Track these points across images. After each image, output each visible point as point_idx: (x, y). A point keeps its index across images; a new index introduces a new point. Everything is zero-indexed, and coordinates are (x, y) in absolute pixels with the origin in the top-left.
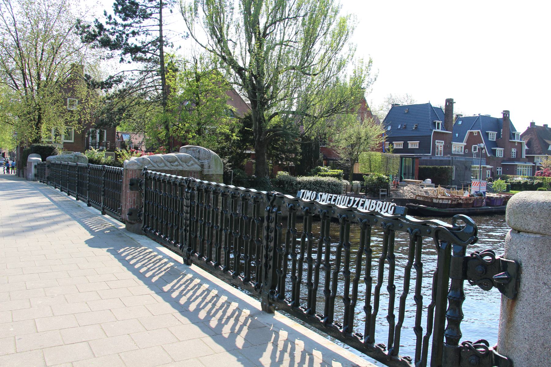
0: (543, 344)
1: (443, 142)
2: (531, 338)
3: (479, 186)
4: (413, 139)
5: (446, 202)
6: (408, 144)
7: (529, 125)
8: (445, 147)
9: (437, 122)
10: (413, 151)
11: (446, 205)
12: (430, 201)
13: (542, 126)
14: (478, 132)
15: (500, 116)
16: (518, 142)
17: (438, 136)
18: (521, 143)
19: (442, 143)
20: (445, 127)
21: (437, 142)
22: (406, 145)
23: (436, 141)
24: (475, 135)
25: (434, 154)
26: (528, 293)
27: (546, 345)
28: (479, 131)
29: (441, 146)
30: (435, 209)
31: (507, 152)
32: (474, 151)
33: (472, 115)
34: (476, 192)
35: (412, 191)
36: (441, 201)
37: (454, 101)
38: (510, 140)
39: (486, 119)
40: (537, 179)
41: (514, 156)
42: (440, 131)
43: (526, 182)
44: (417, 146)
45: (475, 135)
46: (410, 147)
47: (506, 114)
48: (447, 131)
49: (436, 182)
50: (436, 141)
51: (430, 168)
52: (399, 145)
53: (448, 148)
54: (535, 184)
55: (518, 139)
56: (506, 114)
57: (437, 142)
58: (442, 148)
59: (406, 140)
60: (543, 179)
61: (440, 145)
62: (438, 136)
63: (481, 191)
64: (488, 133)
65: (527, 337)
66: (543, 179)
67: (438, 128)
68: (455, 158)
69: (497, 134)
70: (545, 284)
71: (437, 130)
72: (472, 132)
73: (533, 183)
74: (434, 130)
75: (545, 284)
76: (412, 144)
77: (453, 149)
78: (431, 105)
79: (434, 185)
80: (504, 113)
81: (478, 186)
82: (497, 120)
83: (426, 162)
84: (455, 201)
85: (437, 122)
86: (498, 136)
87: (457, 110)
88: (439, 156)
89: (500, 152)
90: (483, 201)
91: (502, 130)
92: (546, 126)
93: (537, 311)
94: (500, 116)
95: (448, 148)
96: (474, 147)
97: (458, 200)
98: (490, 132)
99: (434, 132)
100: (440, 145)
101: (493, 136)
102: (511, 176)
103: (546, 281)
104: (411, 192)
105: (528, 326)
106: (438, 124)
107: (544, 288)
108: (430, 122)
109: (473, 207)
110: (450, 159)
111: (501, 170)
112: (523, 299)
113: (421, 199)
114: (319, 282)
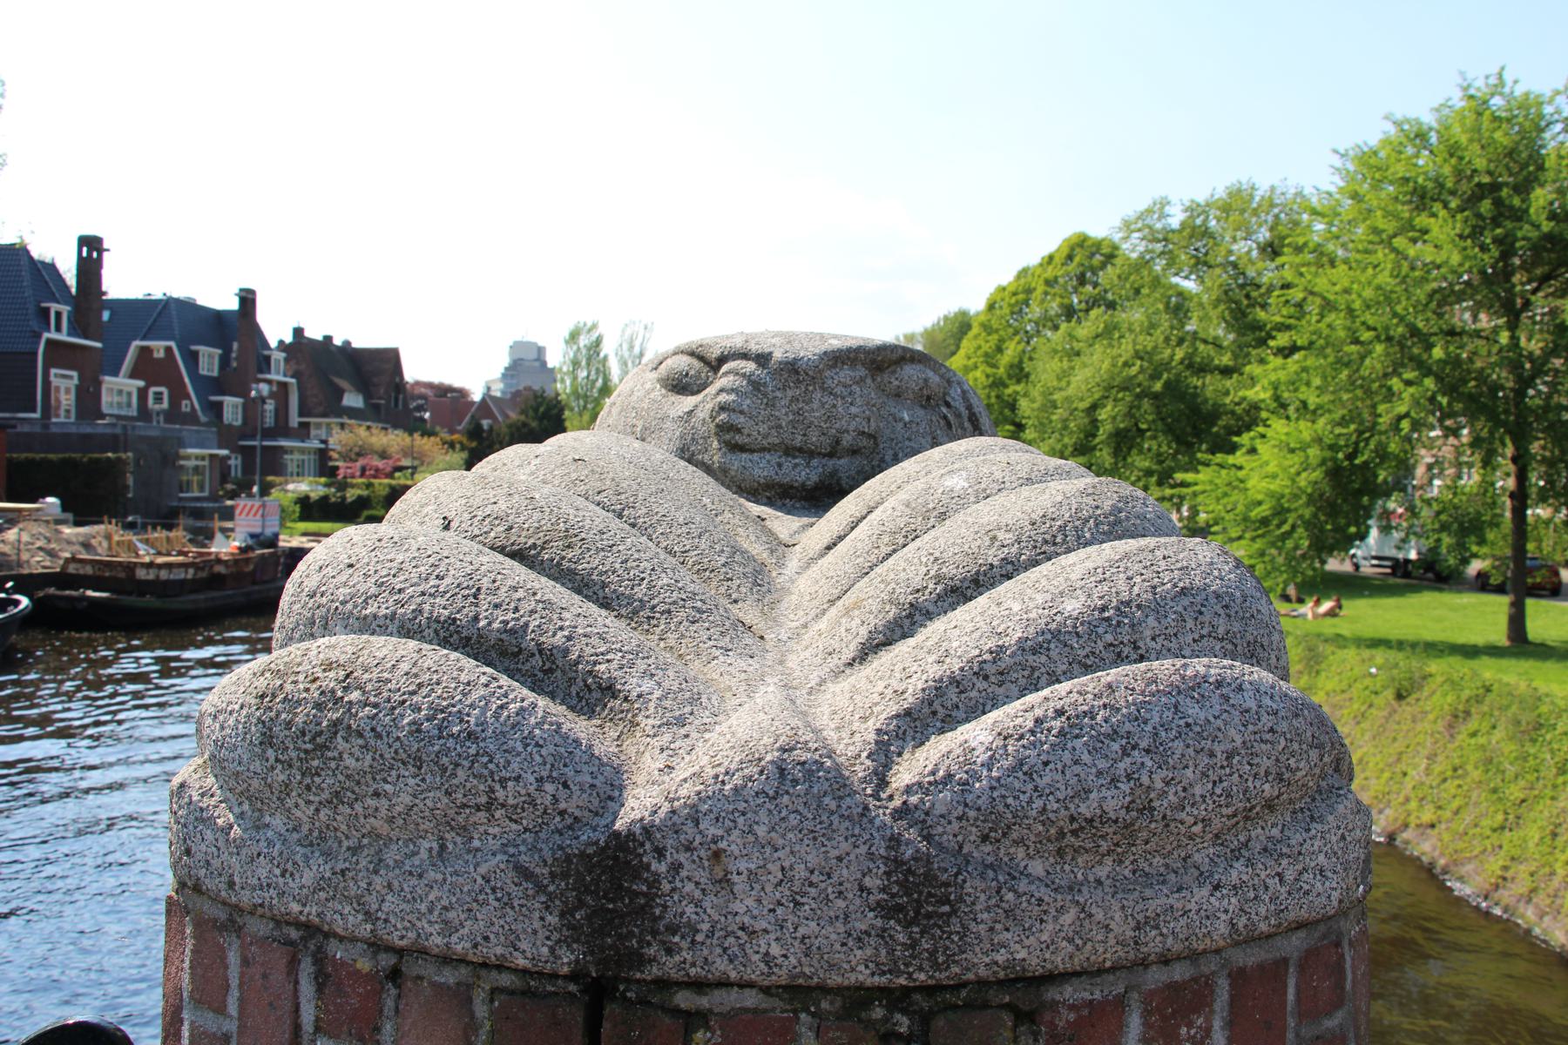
1: (75, 374)
3: (263, 516)
5: (179, 575)
8: (81, 391)
9: (54, 307)
11: (180, 587)
12: (122, 575)
13: (320, 338)
14: (168, 350)
15: (233, 304)
17: (60, 354)
19: (71, 377)
20: (78, 327)
21: (56, 375)
25: (47, 410)
28: (172, 344)
29: (68, 391)
30: (149, 601)
31: (251, 408)
33: (140, 297)
34: (253, 536)
35: (39, 544)
36: (164, 575)
37: (105, 246)
39: (186, 308)
40: (353, 486)
41: (269, 420)
42: (63, 337)
43: (325, 498)
47: (248, 300)
48: (86, 338)
49: (81, 509)
51: (50, 462)
53: (88, 399)
54: (349, 500)
55: (278, 373)
56: (248, 300)
57: (56, 375)
58: (73, 396)
60: (369, 486)
61: (65, 384)
62: (60, 354)
63: (269, 532)
66: (369, 486)
67: (58, 329)
68: (134, 428)
69: (69, 312)
71: (54, 335)
73: (344, 498)
77: (105, 398)
78: (28, 252)
79: (70, 516)
80: (244, 294)
81: (258, 516)
82: (219, 317)
83: (28, 441)
84: (202, 569)
85: (54, 307)
86: (225, 361)
87: (119, 283)
88: (62, 419)
89: (232, 406)
90: (277, 564)
91: (235, 346)
94: (233, 304)
95: (88, 399)
96: (156, 393)
97: (212, 567)
98: (202, 349)
99: (50, 342)
100: (65, 384)
101: (209, 359)
102: (277, 479)
104: (40, 549)
106: (59, 315)
108: (32, 308)
109: (254, 583)
110: (118, 431)
111: (239, 461)
113: (89, 570)
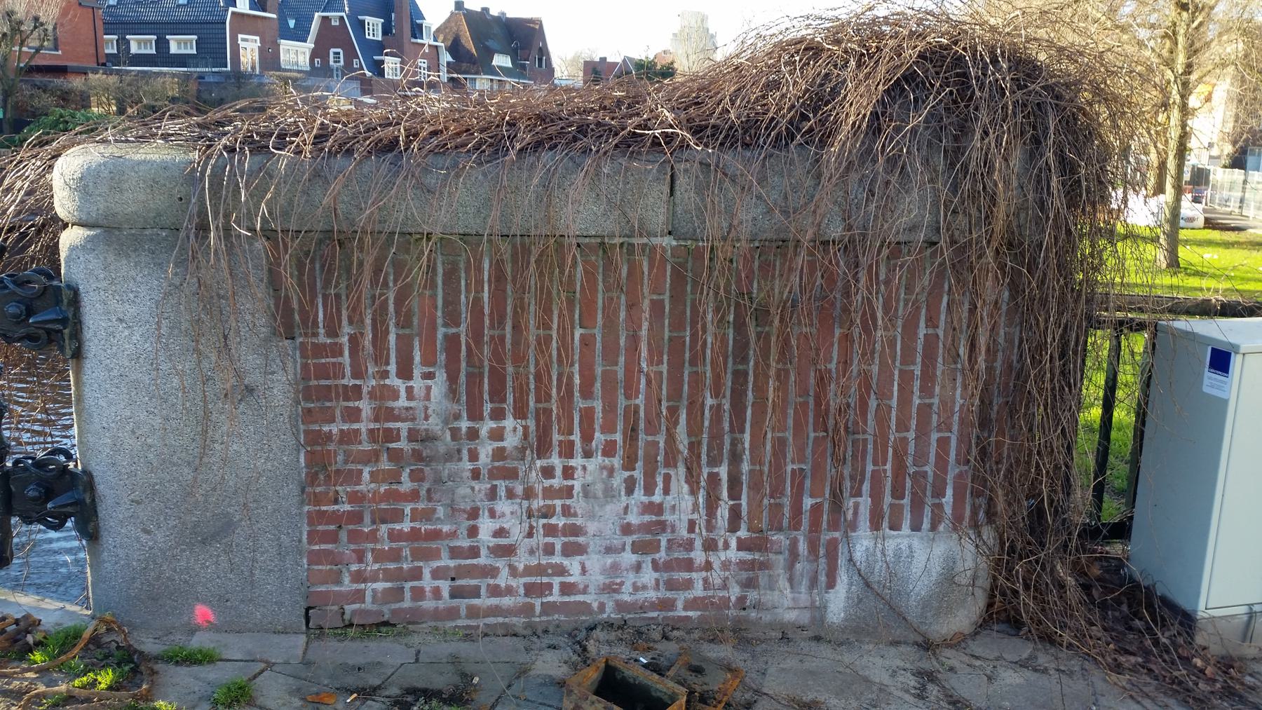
0: (133, 432)
2: (113, 425)
4: (180, 27)
6: (168, 42)
7: (452, 8)
10: (181, 60)
16: (430, 46)
18: (436, 47)
21: (243, 40)
22: (162, 44)
23: (240, 36)
24: (333, 23)
26: (96, 341)
27: (139, 432)
32: (335, 62)
38: (413, 40)
44: (192, 48)
45: (333, 23)
46: (134, 49)
50: (240, 36)
52: (186, 43)
59: (162, 29)
64: (364, 21)
65: (105, 425)
70: (121, 320)
72: (327, 17)
74: (231, 9)
75: (121, 320)
76: (179, 42)
92: (486, 10)
93: (115, 373)
96: (335, 53)
98: (368, 19)
99: (233, 13)
103: (121, 316)
105: (104, 405)
107: (120, 328)
112: (90, 355)
114: (1128, 466)
